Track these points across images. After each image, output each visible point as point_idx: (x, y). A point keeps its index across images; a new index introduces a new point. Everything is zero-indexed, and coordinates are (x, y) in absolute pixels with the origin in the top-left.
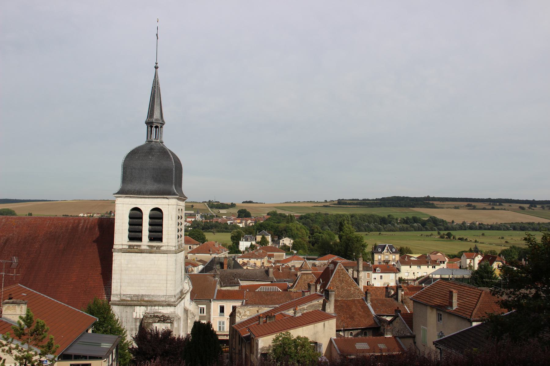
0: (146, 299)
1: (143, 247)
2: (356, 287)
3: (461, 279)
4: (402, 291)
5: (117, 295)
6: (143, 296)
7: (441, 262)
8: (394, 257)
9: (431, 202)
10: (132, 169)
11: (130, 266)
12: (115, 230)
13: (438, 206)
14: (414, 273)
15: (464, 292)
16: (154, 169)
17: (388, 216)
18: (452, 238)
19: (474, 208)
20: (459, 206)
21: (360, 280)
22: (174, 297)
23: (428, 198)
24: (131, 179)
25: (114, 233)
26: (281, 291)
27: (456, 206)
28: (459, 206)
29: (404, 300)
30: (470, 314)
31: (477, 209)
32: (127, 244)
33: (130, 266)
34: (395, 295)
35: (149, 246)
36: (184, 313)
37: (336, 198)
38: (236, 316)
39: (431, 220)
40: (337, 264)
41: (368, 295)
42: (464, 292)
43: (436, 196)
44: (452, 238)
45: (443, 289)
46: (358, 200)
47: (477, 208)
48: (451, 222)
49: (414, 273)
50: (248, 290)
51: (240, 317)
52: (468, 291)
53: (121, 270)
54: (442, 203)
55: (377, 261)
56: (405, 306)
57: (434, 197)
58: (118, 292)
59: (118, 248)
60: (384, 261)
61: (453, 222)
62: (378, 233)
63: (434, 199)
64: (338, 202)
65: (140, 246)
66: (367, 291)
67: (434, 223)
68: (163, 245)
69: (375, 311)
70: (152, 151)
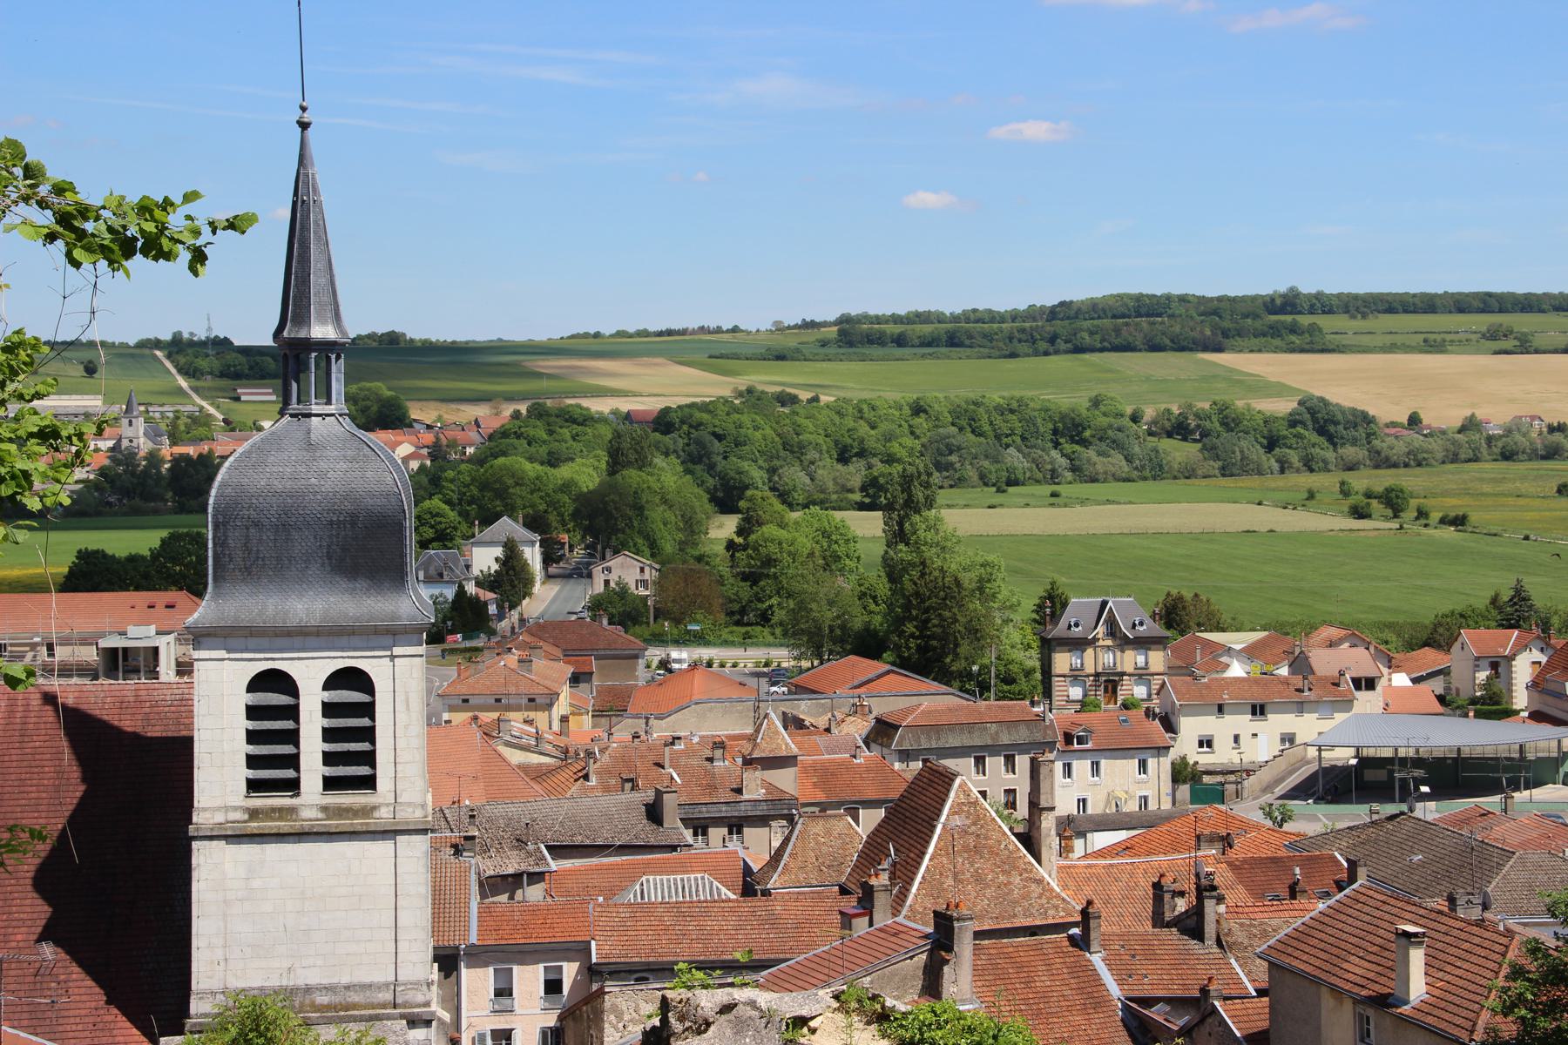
0: (323, 999)
1: (307, 814)
2: (1031, 871)
3: (1449, 761)
4: (1217, 904)
5: (213, 993)
6: (308, 990)
7: (1357, 683)
8: (1141, 660)
9: (1305, 320)
10: (248, 529)
11: (256, 883)
12: (196, 755)
13: (1345, 340)
14: (1236, 738)
15: (1448, 939)
16: (331, 523)
17: (1090, 400)
18: (1410, 514)
19: (1525, 346)
20: (1448, 337)
21: (1043, 844)
22: (425, 987)
23: (1289, 303)
24: (248, 563)
25: (192, 768)
26: (733, 897)
27: (1432, 337)
28: (1448, 337)
29: (1227, 935)
30: (1468, 1025)
31: (1537, 352)
32: (243, 804)
33: (256, 883)
34: (1193, 914)
35: (324, 809)
36: (438, 1034)
37: (828, 312)
38: (606, 1025)
39: (1307, 416)
40: (953, 780)
41: (1091, 921)
42: (1448, 939)
43: (1333, 285)
44: (1410, 514)
45: (1376, 921)
46: (940, 318)
47: (1538, 341)
48: (1404, 420)
49: (1236, 738)
50: (601, 899)
51: (621, 1025)
52: (1463, 935)
53: (225, 901)
54: (1359, 324)
55: (1064, 676)
56: (1233, 961)
57: (1319, 296)
58: (216, 985)
59: (211, 822)
60: (1097, 675)
61: (1414, 420)
62: (1048, 489)
63: (1322, 304)
64: (842, 333)
65: (292, 810)
66: (1087, 907)
67: (1322, 431)
68: (381, 800)
69: (1120, 982)
70: (318, 454)
